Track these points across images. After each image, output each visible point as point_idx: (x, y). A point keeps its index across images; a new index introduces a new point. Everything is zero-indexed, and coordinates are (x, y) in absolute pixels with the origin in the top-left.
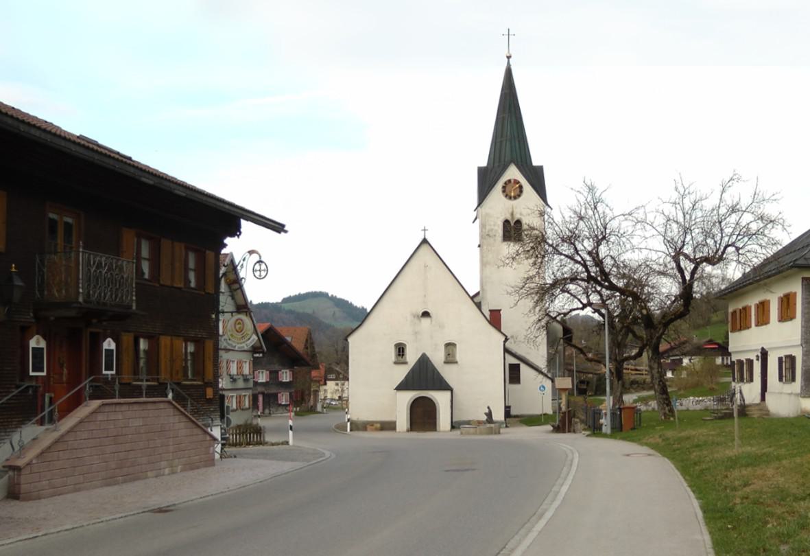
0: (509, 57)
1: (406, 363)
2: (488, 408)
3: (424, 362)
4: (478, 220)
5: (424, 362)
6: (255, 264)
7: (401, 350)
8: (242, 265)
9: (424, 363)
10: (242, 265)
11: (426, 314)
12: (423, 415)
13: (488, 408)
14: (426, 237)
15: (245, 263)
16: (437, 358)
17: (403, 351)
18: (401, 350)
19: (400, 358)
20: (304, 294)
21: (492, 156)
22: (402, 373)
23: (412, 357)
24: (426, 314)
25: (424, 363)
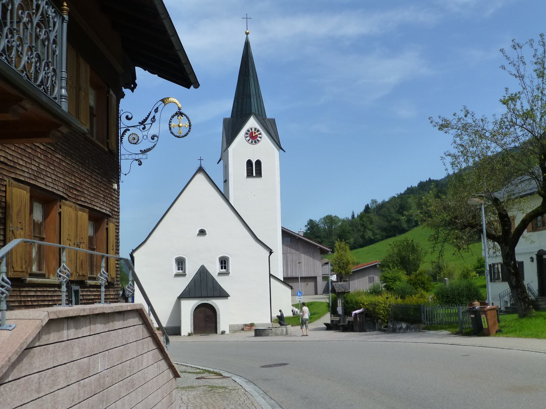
0: (247, 34)
1: (184, 275)
2: (280, 311)
3: (203, 272)
4: (222, 161)
5: (203, 272)
6: (173, 117)
7: (180, 262)
8: (154, 117)
9: (203, 273)
10: (154, 117)
11: (202, 232)
12: (206, 320)
13: (280, 311)
14: (202, 166)
15: (157, 115)
16: (214, 269)
17: (225, 263)
18: (180, 262)
19: (224, 270)
20: (40, 203)
21: (235, 110)
22: (183, 284)
23: (191, 270)
24: (202, 232)
25: (203, 273)
